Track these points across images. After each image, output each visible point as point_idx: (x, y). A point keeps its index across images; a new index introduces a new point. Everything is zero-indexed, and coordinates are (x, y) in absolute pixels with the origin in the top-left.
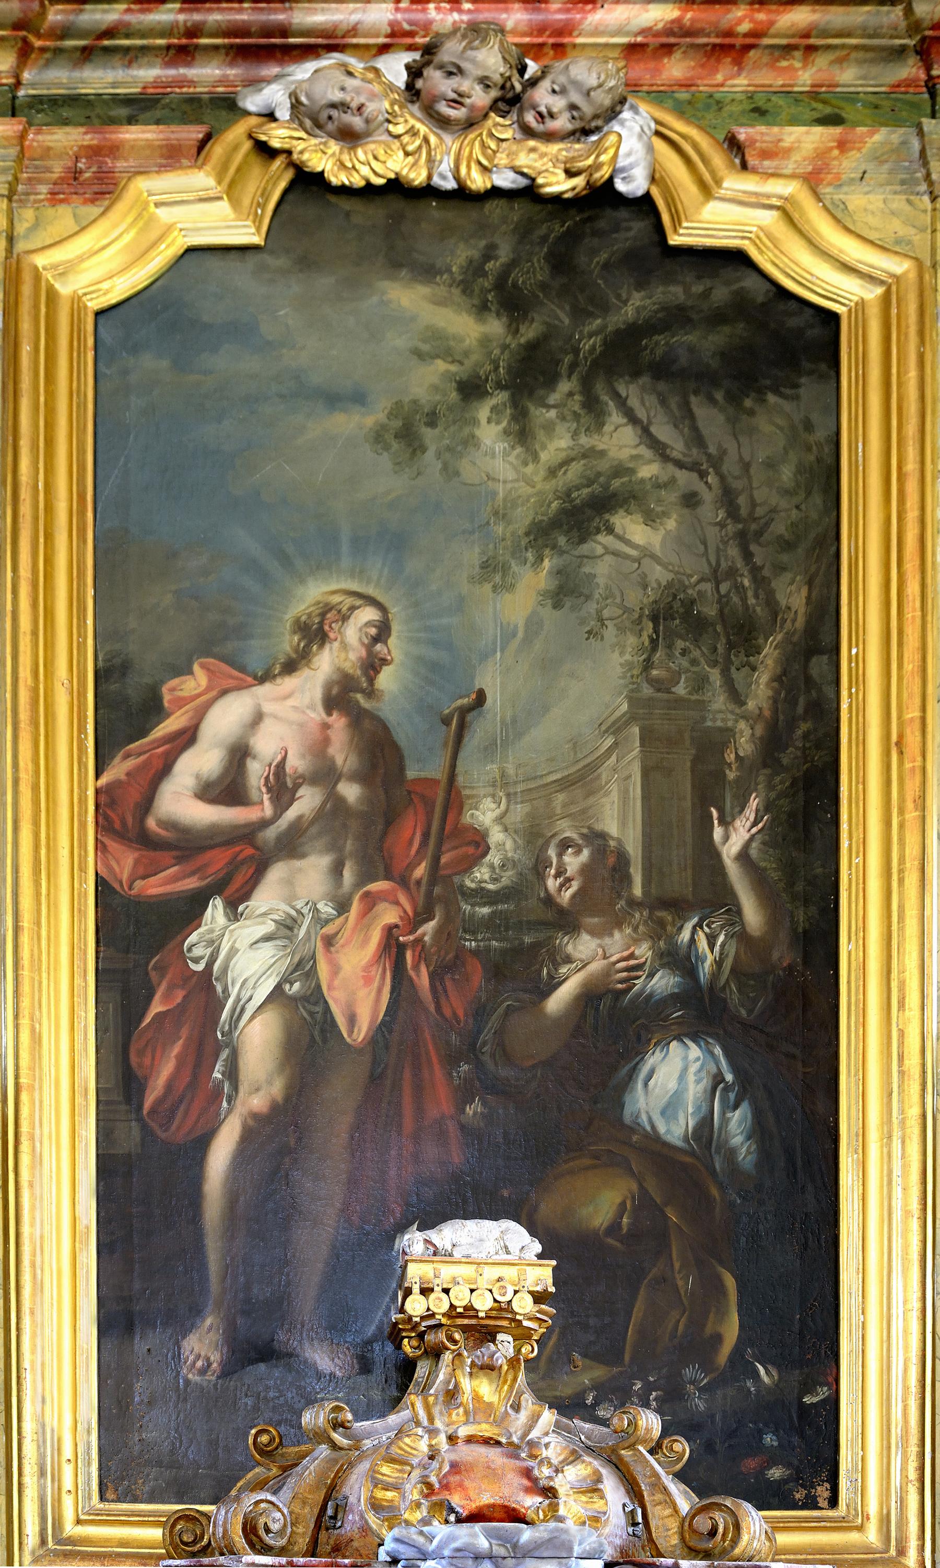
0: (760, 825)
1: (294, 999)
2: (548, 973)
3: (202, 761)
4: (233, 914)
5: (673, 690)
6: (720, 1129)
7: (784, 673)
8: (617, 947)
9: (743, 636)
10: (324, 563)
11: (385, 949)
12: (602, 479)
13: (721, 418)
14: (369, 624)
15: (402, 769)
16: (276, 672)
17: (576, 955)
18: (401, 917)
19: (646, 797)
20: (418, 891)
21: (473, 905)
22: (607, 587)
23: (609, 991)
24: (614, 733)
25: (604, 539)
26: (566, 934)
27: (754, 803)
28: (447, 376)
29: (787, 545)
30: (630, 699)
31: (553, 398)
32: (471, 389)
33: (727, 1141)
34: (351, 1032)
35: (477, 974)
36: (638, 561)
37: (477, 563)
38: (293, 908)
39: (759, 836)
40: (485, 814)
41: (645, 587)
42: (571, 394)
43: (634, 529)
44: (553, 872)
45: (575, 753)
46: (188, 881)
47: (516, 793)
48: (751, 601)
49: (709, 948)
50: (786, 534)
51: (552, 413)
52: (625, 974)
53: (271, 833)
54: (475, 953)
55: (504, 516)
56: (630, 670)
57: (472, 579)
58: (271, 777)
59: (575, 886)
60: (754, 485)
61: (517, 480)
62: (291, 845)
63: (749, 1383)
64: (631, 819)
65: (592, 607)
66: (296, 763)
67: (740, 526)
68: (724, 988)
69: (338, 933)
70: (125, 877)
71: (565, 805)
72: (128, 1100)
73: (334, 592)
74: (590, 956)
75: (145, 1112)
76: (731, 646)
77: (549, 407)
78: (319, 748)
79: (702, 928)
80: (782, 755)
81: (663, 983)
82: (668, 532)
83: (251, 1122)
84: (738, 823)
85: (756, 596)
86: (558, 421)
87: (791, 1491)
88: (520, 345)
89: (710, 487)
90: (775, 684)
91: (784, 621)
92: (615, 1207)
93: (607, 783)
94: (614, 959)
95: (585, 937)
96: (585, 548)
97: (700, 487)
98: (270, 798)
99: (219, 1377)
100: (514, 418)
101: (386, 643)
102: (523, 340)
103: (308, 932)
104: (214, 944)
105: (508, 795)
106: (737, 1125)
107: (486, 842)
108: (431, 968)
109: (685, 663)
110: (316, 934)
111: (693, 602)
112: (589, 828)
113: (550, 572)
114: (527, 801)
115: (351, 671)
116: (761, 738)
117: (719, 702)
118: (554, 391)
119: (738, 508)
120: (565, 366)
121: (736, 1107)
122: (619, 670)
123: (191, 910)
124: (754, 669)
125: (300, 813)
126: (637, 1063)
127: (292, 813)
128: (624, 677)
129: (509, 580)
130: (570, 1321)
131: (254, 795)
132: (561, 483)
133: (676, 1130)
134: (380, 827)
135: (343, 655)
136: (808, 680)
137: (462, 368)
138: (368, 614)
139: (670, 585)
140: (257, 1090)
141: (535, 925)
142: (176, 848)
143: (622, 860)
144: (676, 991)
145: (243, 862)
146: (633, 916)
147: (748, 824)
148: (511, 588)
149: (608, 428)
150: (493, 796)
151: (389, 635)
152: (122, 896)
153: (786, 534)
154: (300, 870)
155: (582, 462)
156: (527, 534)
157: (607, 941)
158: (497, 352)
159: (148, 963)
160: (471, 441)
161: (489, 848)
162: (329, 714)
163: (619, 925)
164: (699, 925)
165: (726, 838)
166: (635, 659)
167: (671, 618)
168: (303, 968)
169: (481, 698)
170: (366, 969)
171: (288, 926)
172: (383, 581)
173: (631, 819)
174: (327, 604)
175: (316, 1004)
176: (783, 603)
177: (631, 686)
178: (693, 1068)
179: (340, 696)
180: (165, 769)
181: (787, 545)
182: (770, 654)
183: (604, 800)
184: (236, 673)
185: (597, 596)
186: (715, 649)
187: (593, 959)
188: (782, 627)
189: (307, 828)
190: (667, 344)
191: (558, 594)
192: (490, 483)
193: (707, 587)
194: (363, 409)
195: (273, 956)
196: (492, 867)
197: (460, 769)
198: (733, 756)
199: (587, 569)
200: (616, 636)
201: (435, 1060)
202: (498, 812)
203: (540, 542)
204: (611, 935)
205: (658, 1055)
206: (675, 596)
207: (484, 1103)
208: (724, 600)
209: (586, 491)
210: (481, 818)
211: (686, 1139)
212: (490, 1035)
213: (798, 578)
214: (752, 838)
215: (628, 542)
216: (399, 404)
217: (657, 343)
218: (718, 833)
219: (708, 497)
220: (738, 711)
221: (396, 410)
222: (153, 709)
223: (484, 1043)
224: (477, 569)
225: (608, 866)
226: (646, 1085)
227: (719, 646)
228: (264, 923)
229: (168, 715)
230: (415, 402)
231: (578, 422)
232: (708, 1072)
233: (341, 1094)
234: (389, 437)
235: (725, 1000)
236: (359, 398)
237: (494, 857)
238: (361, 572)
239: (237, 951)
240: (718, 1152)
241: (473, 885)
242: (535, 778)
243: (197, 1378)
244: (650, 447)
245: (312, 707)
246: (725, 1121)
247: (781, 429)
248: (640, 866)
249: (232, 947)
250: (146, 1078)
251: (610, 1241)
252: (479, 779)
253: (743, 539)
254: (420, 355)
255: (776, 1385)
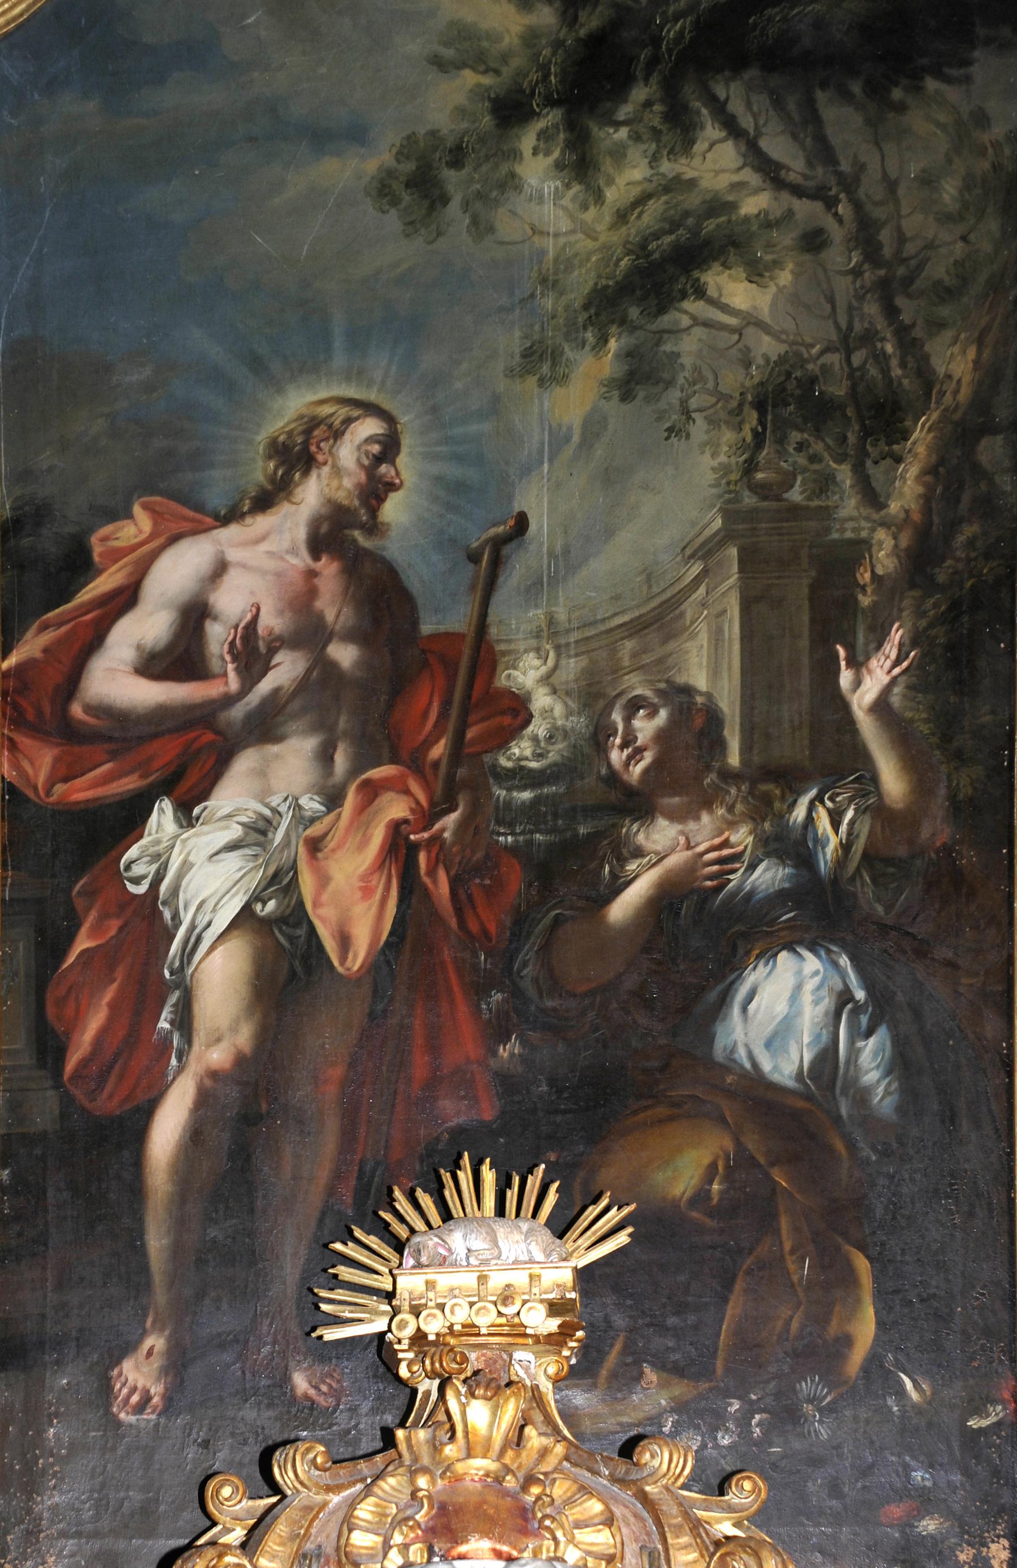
0: (905, 664)
1: (266, 924)
2: (611, 871)
3: (148, 625)
4: (186, 817)
5: (785, 496)
6: (848, 1062)
7: (942, 461)
8: (707, 832)
9: (883, 419)
10: (310, 366)
11: (390, 851)
12: (690, 221)
13: (857, 119)
14: (370, 440)
15: (415, 623)
16: (246, 509)
17: (648, 846)
18: (412, 811)
19: (747, 637)
20: (436, 776)
21: (509, 790)
22: (696, 369)
23: (692, 891)
24: (704, 558)
25: (693, 306)
26: (635, 820)
27: (897, 635)
28: (478, 93)
29: (945, 293)
30: (728, 515)
31: (624, 112)
32: (510, 110)
33: (857, 1079)
34: (343, 959)
35: (515, 880)
36: (739, 332)
37: (517, 351)
38: (267, 805)
39: (902, 679)
40: (526, 674)
41: (747, 364)
42: (648, 104)
43: (734, 290)
44: (618, 741)
45: (650, 587)
46: (125, 780)
47: (568, 645)
48: (896, 372)
49: (831, 829)
50: (947, 279)
51: (623, 133)
52: (715, 868)
53: (238, 712)
54: (512, 850)
55: (555, 283)
56: (725, 475)
57: (510, 373)
58: (238, 641)
59: (648, 757)
60: (903, 213)
61: (573, 232)
62: (265, 726)
63: (891, 1401)
64: (725, 666)
65: (674, 396)
66: (272, 622)
67: (882, 272)
68: (852, 879)
69: (326, 834)
70: (41, 781)
71: (635, 655)
72: (41, 1062)
73: (322, 402)
74: (666, 845)
75: (66, 1077)
76: (866, 433)
77: (617, 124)
78: (302, 600)
79: (822, 802)
80: (937, 570)
81: (768, 876)
82: (780, 290)
83: (208, 1083)
84: (873, 663)
85: (903, 365)
86: (630, 143)
87: (952, 1550)
88: (578, 40)
89: (840, 220)
90: (928, 478)
91: (942, 394)
92: (701, 1171)
93: (692, 623)
94: (701, 848)
95: (662, 822)
96: (665, 320)
97: (829, 223)
98: (236, 669)
99: (159, 1415)
100: (569, 145)
101: (393, 463)
102: (582, 33)
103: (287, 834)
104: (161, 860)
105: (557, 648)
106: (871, 1058)
107: (527, 709)
108: (453, 873)
109: (802, 460)
110: (298, 837)
111: (813, 380)
112: (667, 681)
113: (617, 356)
114: (583, 653)
115: (346, 502)
116: (908, 550)
117: (849, 505)
118: (625, 101)
119: (880, 246)
120: (641, 65)
121: (869, 1033)
122: (711, 477)
123: (129, 818)
124: (899, 460)
125: (276, 685)
126: (732, 983)
127: (265, 686)
128: (716, 485)
129: (561, 370)
130: (640, 1322)
131: (215, 665)
132: (633, 231)
133: (785, 1067)
134: (384, 698)
135: (335, 483)
136: (977, 470)
137: (498, 80)
138: (369, 427)
139: (782, 359)
140: (218, 1040)
141: (591, 811)
142: (110, 739)
143: (714, 719)
144: (787, 885)
145: (199, 751)
146: (728, 792)
147: (888, 664)
148: (563, 380)
149: (699, 147)
150: (538, 650)
151: (398, 453)
152: (35, 804)
153: (947, 279)
154: (277, 756)
155: (664, 198)
156: (586, 307)
157: (692, 825)
158: (546, 52)
159: (70, 889)
160: (511, 183)
161: (531, 716)
162: (316, 558)
163: (708, 804)
164: (819, 798)
165: (857, 683)
166: (733, 460)
167: (784, 403)
168: (282, 881)
169: (522, 523)
170: (365, 877)
171: (259, 830)
172: (389, 383)
173: (725, 666)
174: (313, 418)
175: (297, 925)
176: (941, 371)
177: (727, 496)
178: (810, 985)
179: (332, 535)
180: (94, 640)
181: (945, 293)
182: (921, 438)
183: (688, 644)
184: (191, 514)
185: (681, 381)
186: (845, 438)
187: (672, 850)
188: (938, 402)
189: (287, 702)
190: (785, 19)
191: (628, 382)
192: (536, 239)
193: (834, 359)
194: (363, 151)
195: (240, 869)
196: (535, 739)
197: (491, 618)
198: (867, 576)
199: (668, 347)
200: (707, 432)
201: (456, 989)
202: (544, 670)
203: (603, 318)
204: (697, 818)
205: (762, 970)
206: (789, 374)
207: (524, 1042)
208: (858, 374)
209: (668, 239)
210: (521, 679)
211: (799, 1076)
212: (531, 954)
213: (963, 336)
214: (893, 681)
215: (725, 308)
216: (411, 139)
217: (770, 19)
218: (846, 678)
219: (837, 233)
220: (876, 516)
221: (406, 149)
222: (79, 564)
223: (525, 964)
224: (517, 358)
225: (694, 726)
226: (744, 1009)
227: (849, 435)
228: (227, 828)
229: (100, 572)
230: (433, 133)
231: (658, 141)
232: (831, 990)
233: (328, 1041)
234: (398, 187)
235: (854, 895)
236: (357, 135)
237: (538, 728)
238: (360, 373)
239: (192, 865)
240: (844, 1092)
241: (509, 764)
242: (594, 623)
243: (132, 1419)
244: (758, 169)
245: (293, 551)
246: (854, 1053)
247: (942, 127)
248: (737, 727)
249: (185, 862)
250: (68, 1034)
251: (695, 1214)
252: (518, 629)
253: (886, 292)
254: (440, 64)
255: (930, 1403)
